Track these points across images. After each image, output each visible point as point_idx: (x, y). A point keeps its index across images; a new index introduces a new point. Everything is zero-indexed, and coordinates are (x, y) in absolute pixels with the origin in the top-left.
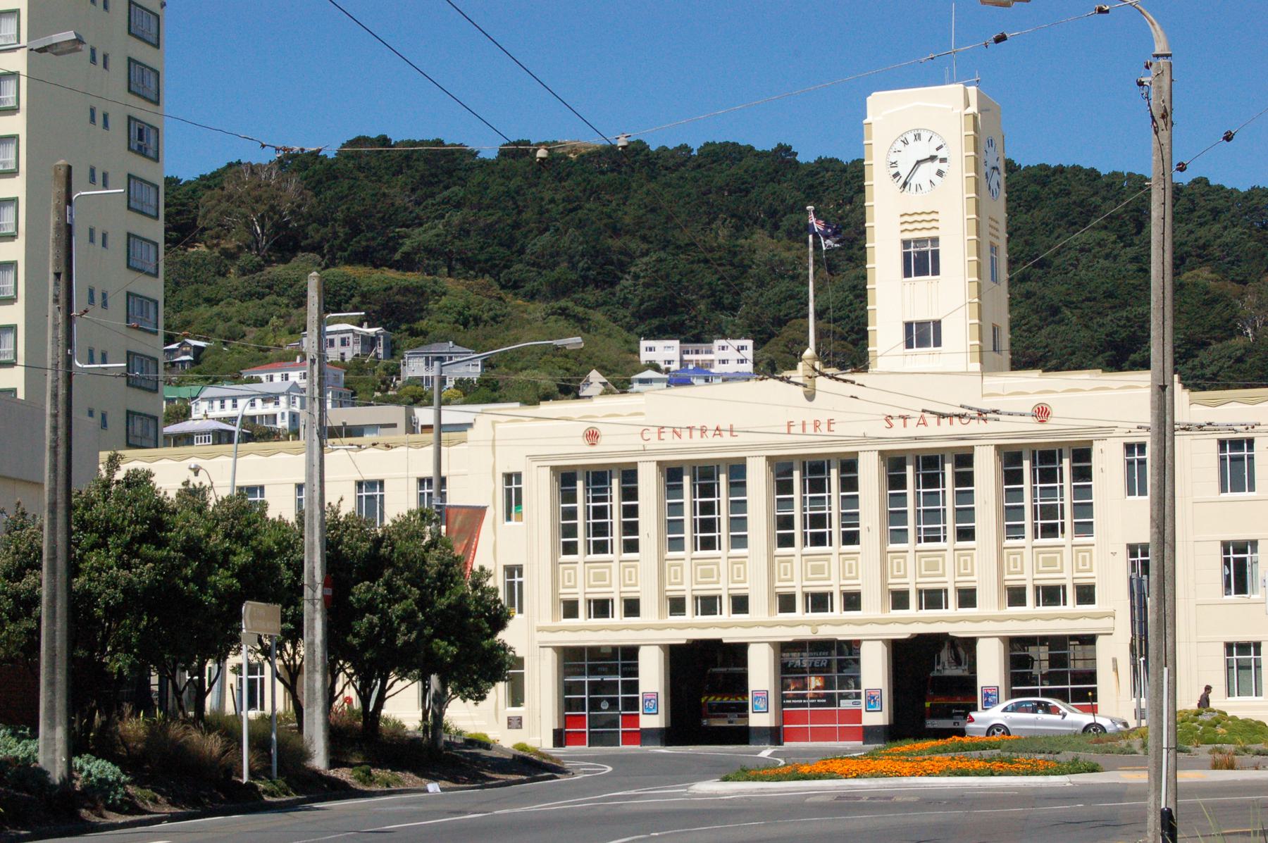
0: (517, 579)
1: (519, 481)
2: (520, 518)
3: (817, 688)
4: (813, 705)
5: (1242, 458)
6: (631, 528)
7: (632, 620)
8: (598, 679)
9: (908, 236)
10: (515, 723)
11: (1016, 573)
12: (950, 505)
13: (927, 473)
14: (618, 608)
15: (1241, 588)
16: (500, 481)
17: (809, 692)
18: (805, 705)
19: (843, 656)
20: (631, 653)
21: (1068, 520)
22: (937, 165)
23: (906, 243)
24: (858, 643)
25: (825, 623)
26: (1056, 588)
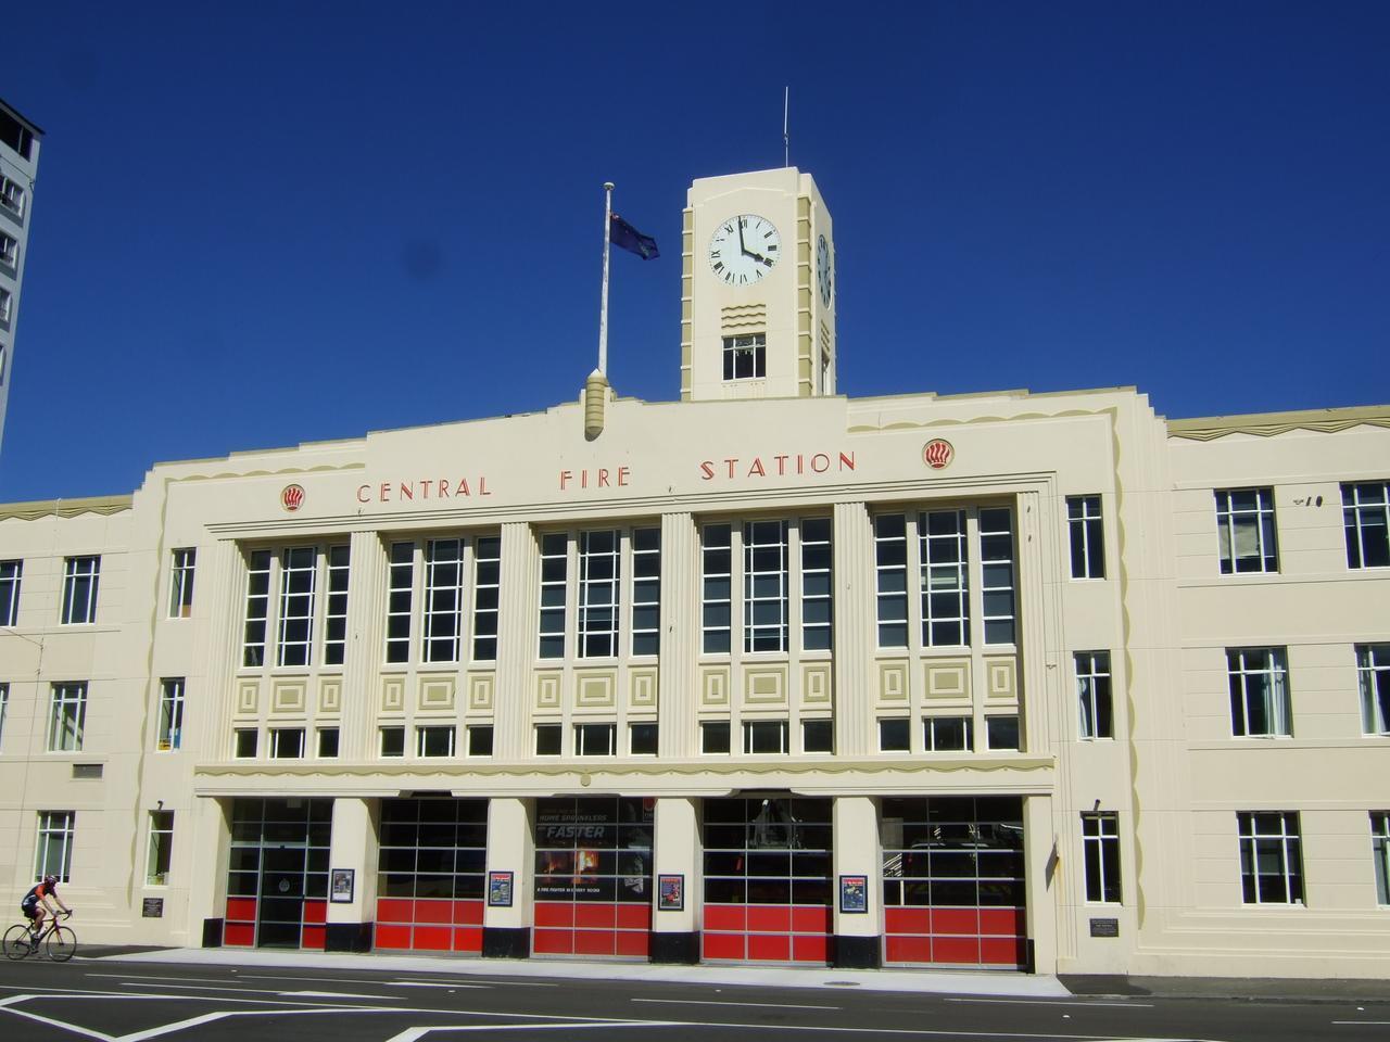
0: (177, 698)
1: (192, 561)
2: (187, 613)
3: (587, 870)
4: (580, 897)
5: (88, 579)
6: (487, 623)
7: (481, 760)
8: (277, 846)
9: (730, 332)
10: (153, 908)
11: (332, 710)
12: (797, 595)
13: (768, 543)
14: (463, 740)
15: (1105, 729)
16: (170, 561)
17: (576, 877)
18: (568, 896)
19: (628, 819)
20: (321, 810)
21: (979, 618)
22: (760, 266)
23: (728, 341)
24: (650, 802)
25: (778, 768)
26: (774, 725)
